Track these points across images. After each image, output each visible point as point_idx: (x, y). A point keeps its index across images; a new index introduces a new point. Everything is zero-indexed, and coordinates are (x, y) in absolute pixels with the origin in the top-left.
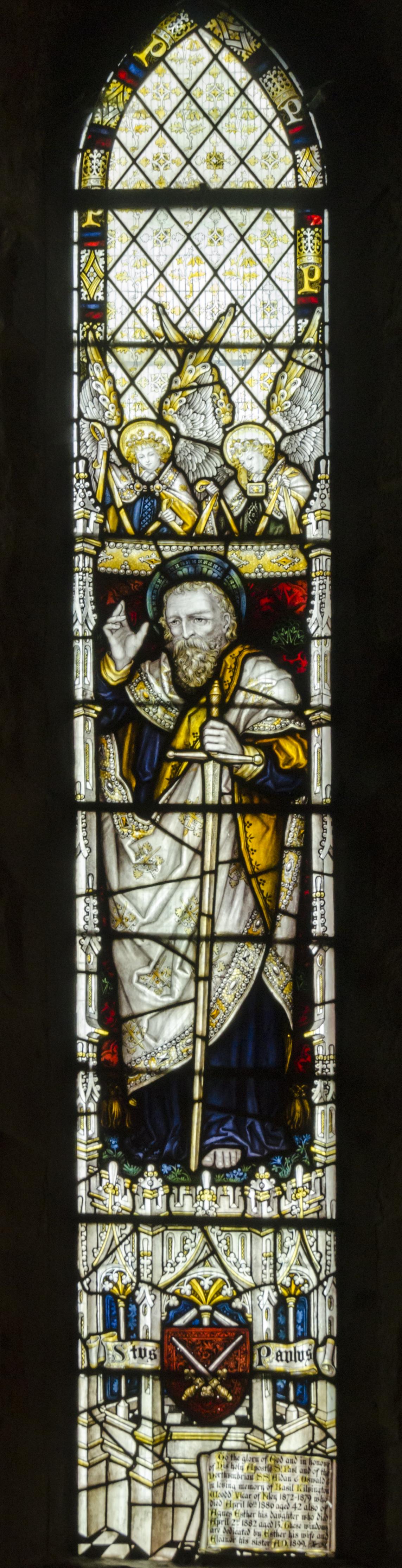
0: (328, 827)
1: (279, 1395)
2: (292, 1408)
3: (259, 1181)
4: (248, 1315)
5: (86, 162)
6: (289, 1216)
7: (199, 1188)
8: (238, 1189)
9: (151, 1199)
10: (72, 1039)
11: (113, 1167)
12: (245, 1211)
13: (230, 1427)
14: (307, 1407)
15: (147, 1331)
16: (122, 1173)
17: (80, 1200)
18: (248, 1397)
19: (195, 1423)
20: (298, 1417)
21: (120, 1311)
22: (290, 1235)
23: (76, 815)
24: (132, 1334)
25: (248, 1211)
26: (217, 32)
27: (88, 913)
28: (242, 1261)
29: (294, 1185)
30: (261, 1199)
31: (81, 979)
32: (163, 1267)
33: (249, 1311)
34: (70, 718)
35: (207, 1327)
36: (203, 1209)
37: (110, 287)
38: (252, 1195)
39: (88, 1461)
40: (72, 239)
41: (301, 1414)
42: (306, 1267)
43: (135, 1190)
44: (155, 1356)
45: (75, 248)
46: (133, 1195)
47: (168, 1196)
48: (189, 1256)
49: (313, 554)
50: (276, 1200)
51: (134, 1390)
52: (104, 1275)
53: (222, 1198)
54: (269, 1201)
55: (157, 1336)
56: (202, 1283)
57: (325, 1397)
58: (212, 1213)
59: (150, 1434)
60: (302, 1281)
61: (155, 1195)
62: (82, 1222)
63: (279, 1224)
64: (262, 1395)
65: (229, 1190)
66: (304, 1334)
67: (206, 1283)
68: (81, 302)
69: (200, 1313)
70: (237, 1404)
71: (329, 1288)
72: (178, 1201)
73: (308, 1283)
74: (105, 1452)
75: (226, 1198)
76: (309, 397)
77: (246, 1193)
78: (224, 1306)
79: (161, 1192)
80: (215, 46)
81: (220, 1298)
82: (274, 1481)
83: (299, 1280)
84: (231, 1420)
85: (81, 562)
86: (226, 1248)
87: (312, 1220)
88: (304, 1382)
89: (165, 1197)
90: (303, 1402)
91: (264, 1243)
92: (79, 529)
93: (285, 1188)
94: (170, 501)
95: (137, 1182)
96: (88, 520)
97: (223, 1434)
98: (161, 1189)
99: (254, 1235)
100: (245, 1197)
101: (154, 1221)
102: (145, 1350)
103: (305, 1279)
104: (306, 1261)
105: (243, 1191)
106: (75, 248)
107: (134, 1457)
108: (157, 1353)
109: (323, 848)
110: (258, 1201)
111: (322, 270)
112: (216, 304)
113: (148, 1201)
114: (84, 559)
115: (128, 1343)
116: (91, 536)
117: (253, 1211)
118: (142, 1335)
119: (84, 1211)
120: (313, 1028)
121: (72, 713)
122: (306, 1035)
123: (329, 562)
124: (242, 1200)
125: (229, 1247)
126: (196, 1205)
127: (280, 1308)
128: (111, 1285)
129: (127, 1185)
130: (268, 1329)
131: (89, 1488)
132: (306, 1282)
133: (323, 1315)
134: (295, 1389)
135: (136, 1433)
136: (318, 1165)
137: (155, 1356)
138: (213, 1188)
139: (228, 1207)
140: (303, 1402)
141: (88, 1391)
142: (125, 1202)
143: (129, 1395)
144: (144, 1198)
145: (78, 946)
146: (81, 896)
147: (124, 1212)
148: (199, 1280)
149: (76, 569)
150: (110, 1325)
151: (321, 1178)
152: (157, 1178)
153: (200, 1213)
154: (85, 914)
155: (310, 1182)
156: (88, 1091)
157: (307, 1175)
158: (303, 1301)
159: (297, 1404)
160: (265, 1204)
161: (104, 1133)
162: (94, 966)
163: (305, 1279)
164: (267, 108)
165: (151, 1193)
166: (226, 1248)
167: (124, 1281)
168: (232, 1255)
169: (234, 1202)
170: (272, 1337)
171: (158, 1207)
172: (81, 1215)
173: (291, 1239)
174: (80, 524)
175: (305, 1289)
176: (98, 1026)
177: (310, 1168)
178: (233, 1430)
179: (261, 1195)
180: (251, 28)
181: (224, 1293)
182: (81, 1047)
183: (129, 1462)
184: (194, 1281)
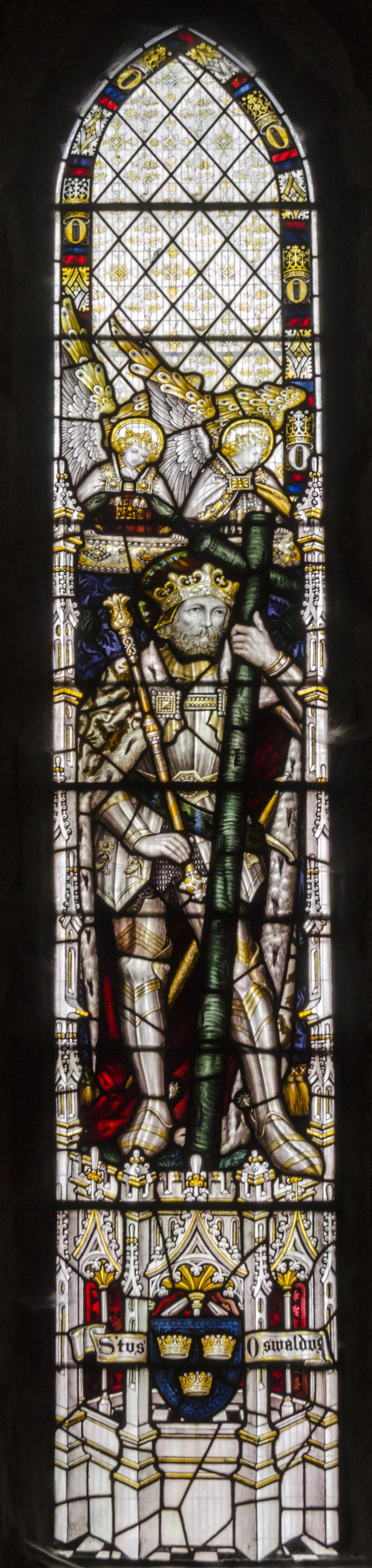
0: (324, 806)
1: (275, 1385)
5: (67, 188)
6: (283, 1200)
7: (189, 1174)
8: (229, 1174)
9: (139, 1188)
10: (51, 1019)
11: (95, 1152)
12: (237, 1194)
13: (220, 1423)
18: (240, 1391)
19: (182, 1419)
22: (285, 1219)
24: (116, 1325)
31: (58, 605)
32: (150, 1255)
34: (49, 704)
35: (197, 1317)
36: (193, 1195)
37: (94, 281)
42: (302, 1253)
44: (143, 1349)
45: (57, 266)
47: (156, 1183)
50: (269, 1183)
51: (118, 1383)
55: (144, 1328)
56: (192, 1269)
58: (202, 1199)
60: (298, 1267)
64: (257, 1391)
65: (221, 1177)
66: (300, 1323)
67: (196, 1269)
69: (190, 1302)
72: (167, 1188)
73: (304, 1270)
74: (86, 1453)
75: (218, 1185)
77: (237, 1177)
79: (150, 1179)
83: (295, 1266)
84: (222, 1416)
85: (62, 561)
89: (152, 1186)
90: (301, 1391)
94: (116, 1250)
97: (213, 1432)
100: (237, 1183)
101: (139, 1207)
103: (301, 1266)
104: (304, 1248)
105: (234, 1176)
106: (57, 266)
107: (118, 1458)
108: (145, 1346)
109: (317, 826)
110: (251, 1185)
111: (310, 286)
112: (206, 244)
114: (67, 1025)
117: (245, 1196)
119: (64, 1198)
120: (308, 1008)
121: (52, 548)
122: (301, 1015)
124: (233, 1186)
126: (185, 1192)
131: (68, 1501)
132: (302, 1268)
133: (323, 1304)
135: (121, 1432)
137: (143, 1349)
138: (204, 1174)
141: (67, 1388)
142: (111, 1190)
145: (59, 924)
146: (61, 942)
147: (107, 1199)
148: (189, 1266)
150: (92, 1317)
153: (190, 1199)
158: (300, 1289)
159: (294, 1394)
160: (258, 1188)
161: (85, 1110)
164: (252, 131)
168: (224, 1239)
169: (225, 1188)
170: (265, 1326)
171: (145, 1195)
172: (61, 1201)
173: (286, 1223)
175: (302, 1276)
178: (224, 1426)
180: (238, 62)
181: (215, 1279)
182: (61, 1028)
183: (113, 1463)
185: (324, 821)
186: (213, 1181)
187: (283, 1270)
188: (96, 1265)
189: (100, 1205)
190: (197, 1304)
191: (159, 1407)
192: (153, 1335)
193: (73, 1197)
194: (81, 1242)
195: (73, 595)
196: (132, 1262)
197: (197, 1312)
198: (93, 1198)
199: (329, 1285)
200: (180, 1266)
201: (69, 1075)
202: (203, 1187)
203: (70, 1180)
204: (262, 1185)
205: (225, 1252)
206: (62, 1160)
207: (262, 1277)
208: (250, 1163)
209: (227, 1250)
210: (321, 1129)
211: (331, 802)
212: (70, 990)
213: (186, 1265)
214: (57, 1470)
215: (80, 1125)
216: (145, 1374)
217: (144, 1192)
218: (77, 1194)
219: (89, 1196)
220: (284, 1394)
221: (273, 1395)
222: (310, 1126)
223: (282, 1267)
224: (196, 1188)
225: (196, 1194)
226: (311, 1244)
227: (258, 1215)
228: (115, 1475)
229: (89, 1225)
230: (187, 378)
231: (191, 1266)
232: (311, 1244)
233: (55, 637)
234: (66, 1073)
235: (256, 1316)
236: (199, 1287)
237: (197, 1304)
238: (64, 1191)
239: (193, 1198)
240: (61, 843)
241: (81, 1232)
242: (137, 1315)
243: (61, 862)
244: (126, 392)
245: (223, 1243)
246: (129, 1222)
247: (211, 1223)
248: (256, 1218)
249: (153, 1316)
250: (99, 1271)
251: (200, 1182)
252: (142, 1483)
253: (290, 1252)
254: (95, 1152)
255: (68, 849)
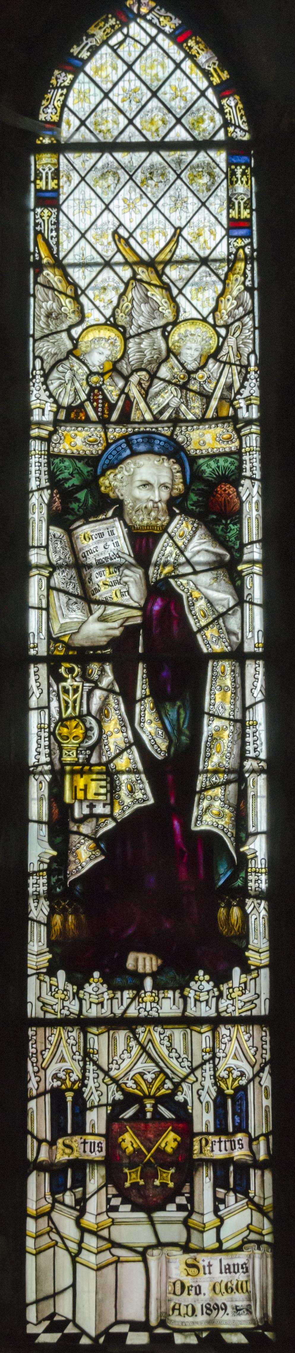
1: (220, 1182)
2: (231, 1194)
3: (199, 983)
4: (189, 1107)
9: (97, 1004)
11: (61, 974)
12: (185, 1009)
14: (246, 1194)
15: (93, 1126)
16: (69, 979)
17: (29, 1006)
20: (236, 1202)
21: (68, 1109)
23: (28, 668)
25: (188, 1010)
26: (155, 21)
27: (39, 753)
28: (183, 1056)
29: (230, 985)
30: (201, 999)
33: (190, 1103)
36: (145, 1010)
38: (192, 995)
39: (35, 1249)
40: (30, 178)
41: (239, 1199)
43: (81, 996)
46: (80, 1000)
48: (133, 1053)
49: (245, 431)
51: (80, 1181)
52: (54, 1072)
53: (164, 1000)
54: (207, 1001)
55: (103, 1131)
56: (145, 1077)
57: (262, 1185)
58: (154, 1014)
59: (94, 1221)
61: (101, 1000)
62: (31, 1026)
63: (216, 1022)
68: (37, 191)
69: (143, 1107)
70: (178, 1191)
71: (266, 1079)
76: (240, 295)
78: (168, 1100)
80: (153, 32)
81: (163, 1091)
82: (216, 1268)
85: (35, 446)
86: (169, 1044)
87: (246, 1017)
88: (242, 1169)
91: (202, 1039)
92: (36, 416)
93: (222, 988)
95: (83, 988)
96: (43, 410)
98: (106, 994)
99: (194, 1033)
100: (185, 998)
102: (94, 1143)
104: (241, 1054)
113: (94, 1006)
115: (77, 1138)
116: (46, 423)
117: (192, 1011)
118: (88, 1130)
123: (258, 438)
124: (181, 1001)
125: (171, 1044)
127: (221, 1098)
128: (59, 1083)
129: (75, 991)
130: (267, 1106)
132: (242, 1074)
133: (259, 1105)
134: (232, 1177)
136: (252, 967)
139: (169, 1006)
140: (242, 1188)
141: (36, 1189)
142: (74, 1007)
143: (74, 1187)
144: (91, 1003)
149: (33, 452)
151: (255, 978)
152: (102, 984)
153: (143, 1014)
154: (38, 805)
155: (245, 983)
156: (37, 885)
157: (244, 976)
160: (204, 1004)
162: (44, 484)
163: (241, 1072)
165: (97, 998)
166: (169, 1044)
167: (72, 1079)
169: (174, 1004)
170: (212, 1129)
171: (103, 1011)
174: (36, 412)
176: (49, 848)
177: (246, 970)
179: (201, 995)
184: (138, 1076)
185: (260, 684)
186: (163, 998)
187: (226, 1076)
188: (62, 1075)
189: (65, 1022)
190: (149, 1107)
191: (114, 1196)
192: (111, 1137)
193: (41, 1014)
194: (47, 1055)
195: (48, 484)
196: (91, 1079)
197: (149, 1115)
198: (59, 1016)
199: (266, 1088)
200: (134, 1075)
201: (39, 909)
202: (154, 1002)
203: (39, 999)
204: (207, 1001)
205: (175, 1061)
206: (32, 983)
207: (208, 1083)
208: (196, 982)
209: (177, 1059)
210: (258, 952)
211: (266, 667)
212: (41, 833)
213: (139, 1073)
214: (28, 1256)
215: (50, 952)
216: (103, 1171)
217: (102, 1007)
218: (45, 1012)
219: (56, 1013)
220: (228, 1189)
221: (217, 1189)
222: (248, 949)
223: (224, 1074)
224: (148, 1004)
225: (148, 1008)
226: (250, 1053)
227: (205, 1028)
228: (78, 1259)
229: (54, 1039)
230: (71, 1289)
231: (145, 1074)
232: (250, 1053)
233: (31, 516)
234: (36, 907)
235: (203, 1119)
236: (152, 1093)
237: (149, 1107)
238: (34, 1010)
239: (146, 1013)
240: (33, 702)
241: (48, 1046)
242: (96, 1119)
243: (34, 719)
244: (95, 95)
245: (174, 1054)
246: (89, 1036)
247: (162, 1037)
248: (202, 1031)
249: (112, 1119)
250: (65, 1080)
251: (152, 998)
252: (99, 1249)
253: (231, 1062)
254: (61, 974)
255: (40, 708)
